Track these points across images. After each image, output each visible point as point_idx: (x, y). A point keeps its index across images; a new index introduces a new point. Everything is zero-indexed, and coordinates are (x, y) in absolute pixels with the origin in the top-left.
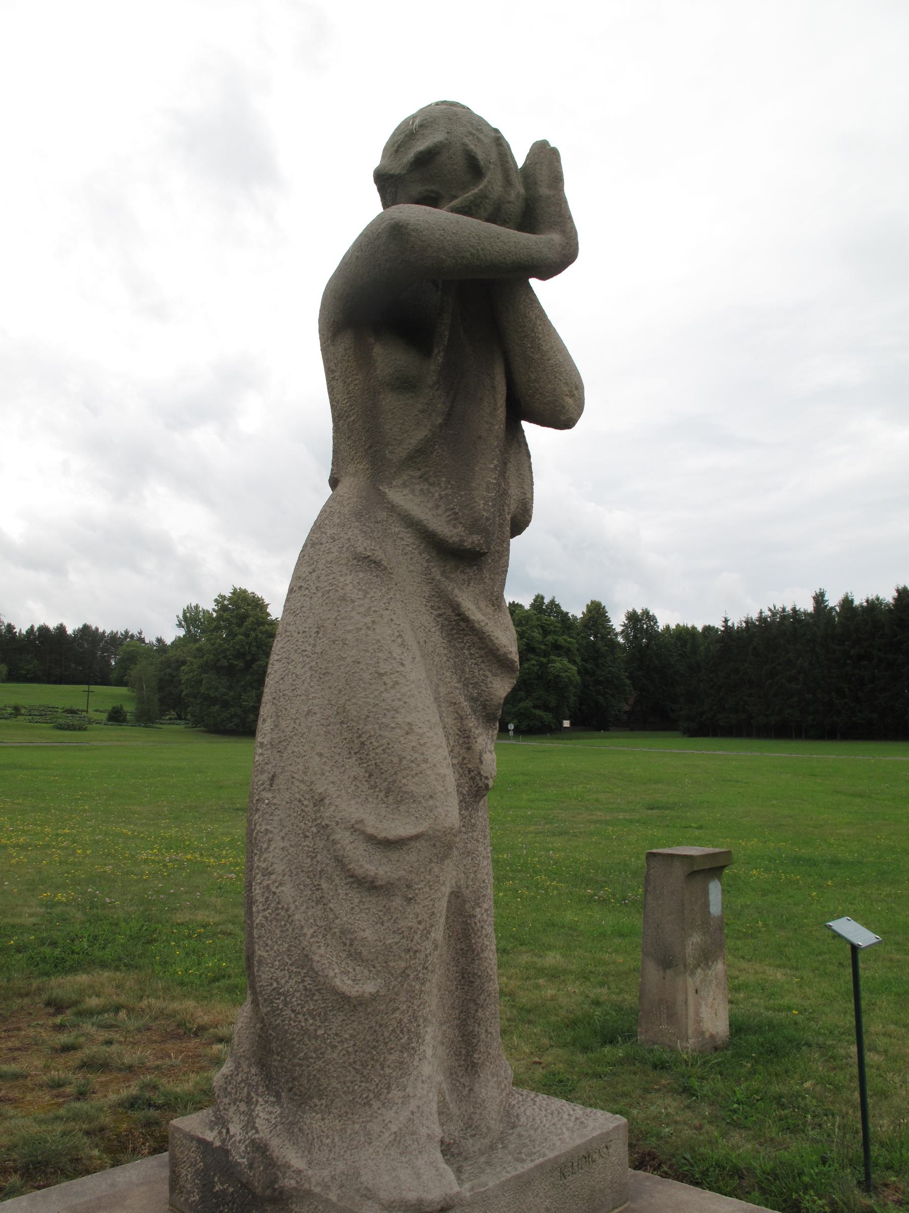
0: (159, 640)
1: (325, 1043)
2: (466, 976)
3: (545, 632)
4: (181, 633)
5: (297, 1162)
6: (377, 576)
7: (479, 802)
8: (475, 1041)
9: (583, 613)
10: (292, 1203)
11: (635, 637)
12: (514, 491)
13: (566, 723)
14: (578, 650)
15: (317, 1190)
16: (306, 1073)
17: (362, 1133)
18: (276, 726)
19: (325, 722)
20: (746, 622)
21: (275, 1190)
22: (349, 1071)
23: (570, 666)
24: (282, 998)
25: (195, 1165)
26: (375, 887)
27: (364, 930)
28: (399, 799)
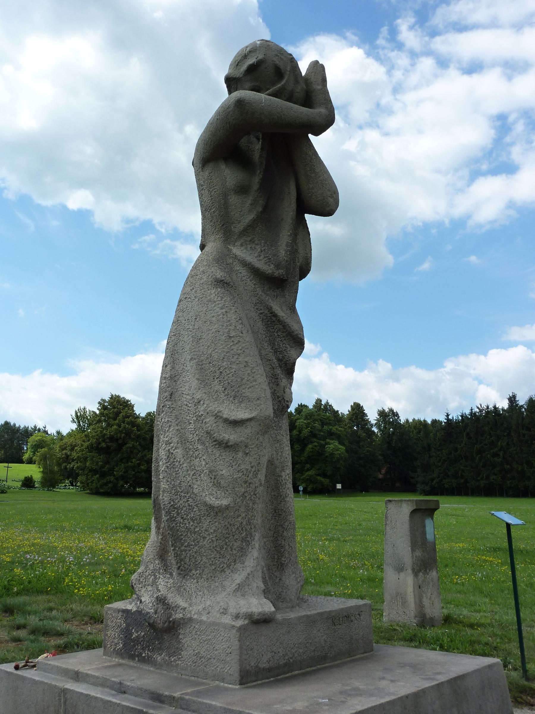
0: (58, 433)
1: (200, 536)
2: (277, 511)
3: (323, 424)
4: (74, 426)
5: (182, 603)
6: (228, 291)
7: (283, 415)
8: (282, 550)
9: (349, 411)
10: (179, 629)
11: (385, 427)
12: (301, 251)
13: (339, 486)
14: (346, 436)
15: (196, 616)
16: (188, 555)
17: (220, 586)
18: (173, 368)
19: (200, 363)
20: (462, 416)
21: (170, 622)
22: (213, 552)
23: (340, 447)
24: (176, 510)
25: (121, 626)
26: (228, 447)
27: (222, 470)
28: (241, 400)
